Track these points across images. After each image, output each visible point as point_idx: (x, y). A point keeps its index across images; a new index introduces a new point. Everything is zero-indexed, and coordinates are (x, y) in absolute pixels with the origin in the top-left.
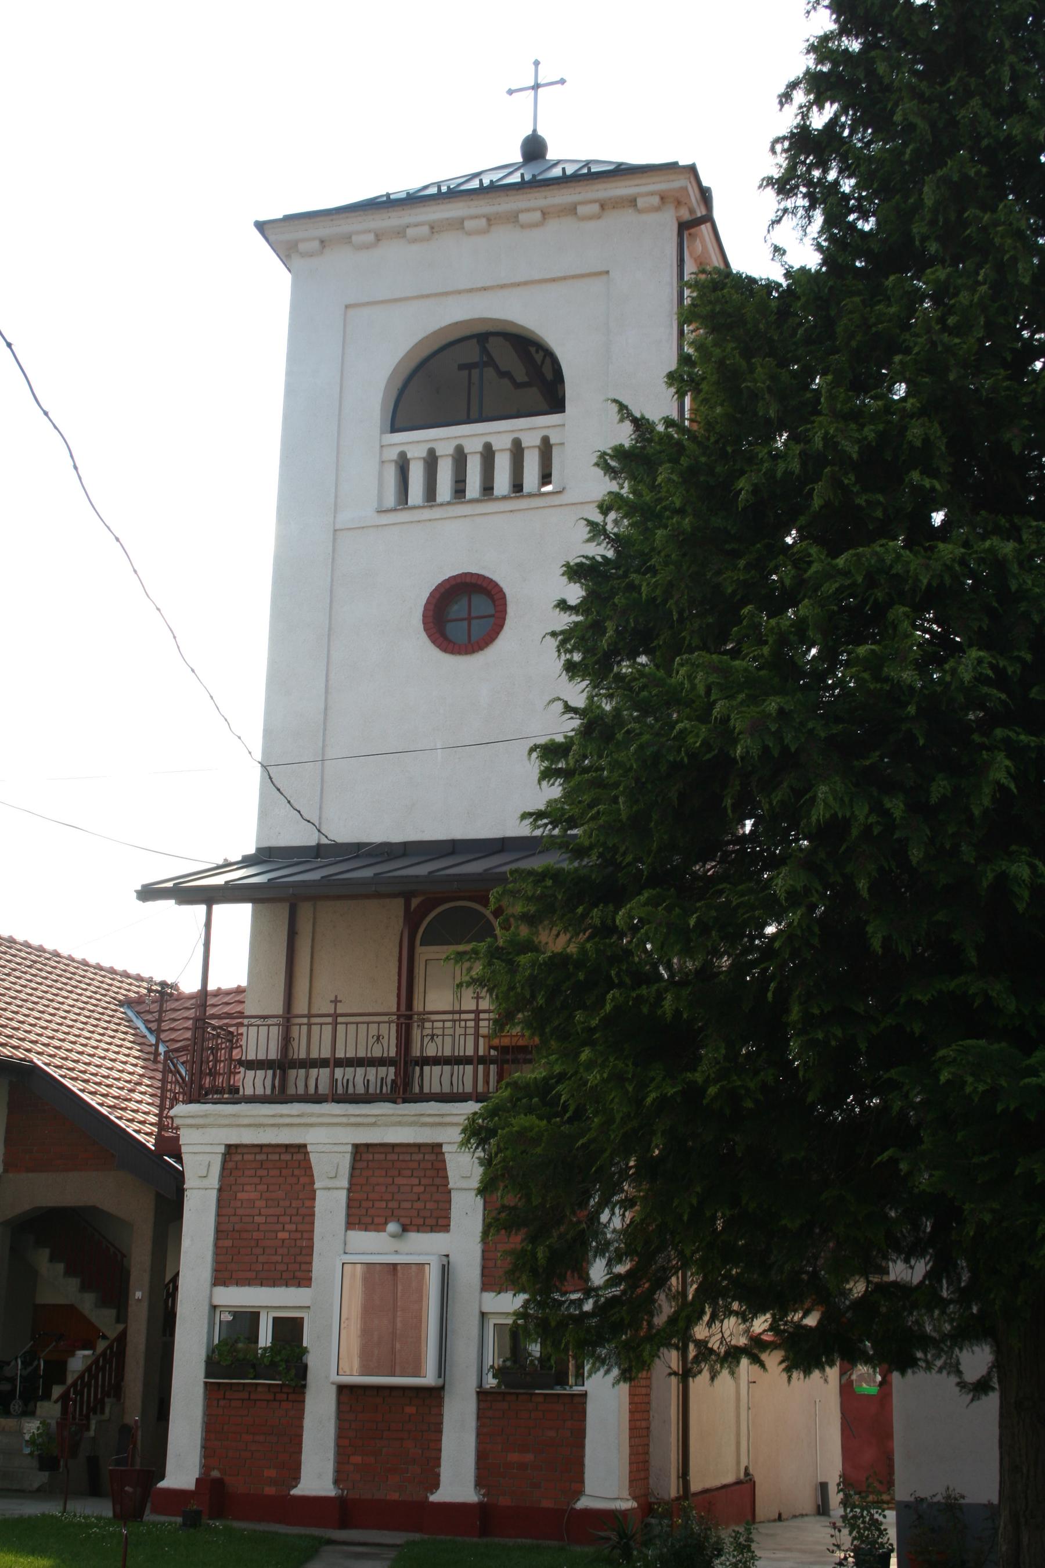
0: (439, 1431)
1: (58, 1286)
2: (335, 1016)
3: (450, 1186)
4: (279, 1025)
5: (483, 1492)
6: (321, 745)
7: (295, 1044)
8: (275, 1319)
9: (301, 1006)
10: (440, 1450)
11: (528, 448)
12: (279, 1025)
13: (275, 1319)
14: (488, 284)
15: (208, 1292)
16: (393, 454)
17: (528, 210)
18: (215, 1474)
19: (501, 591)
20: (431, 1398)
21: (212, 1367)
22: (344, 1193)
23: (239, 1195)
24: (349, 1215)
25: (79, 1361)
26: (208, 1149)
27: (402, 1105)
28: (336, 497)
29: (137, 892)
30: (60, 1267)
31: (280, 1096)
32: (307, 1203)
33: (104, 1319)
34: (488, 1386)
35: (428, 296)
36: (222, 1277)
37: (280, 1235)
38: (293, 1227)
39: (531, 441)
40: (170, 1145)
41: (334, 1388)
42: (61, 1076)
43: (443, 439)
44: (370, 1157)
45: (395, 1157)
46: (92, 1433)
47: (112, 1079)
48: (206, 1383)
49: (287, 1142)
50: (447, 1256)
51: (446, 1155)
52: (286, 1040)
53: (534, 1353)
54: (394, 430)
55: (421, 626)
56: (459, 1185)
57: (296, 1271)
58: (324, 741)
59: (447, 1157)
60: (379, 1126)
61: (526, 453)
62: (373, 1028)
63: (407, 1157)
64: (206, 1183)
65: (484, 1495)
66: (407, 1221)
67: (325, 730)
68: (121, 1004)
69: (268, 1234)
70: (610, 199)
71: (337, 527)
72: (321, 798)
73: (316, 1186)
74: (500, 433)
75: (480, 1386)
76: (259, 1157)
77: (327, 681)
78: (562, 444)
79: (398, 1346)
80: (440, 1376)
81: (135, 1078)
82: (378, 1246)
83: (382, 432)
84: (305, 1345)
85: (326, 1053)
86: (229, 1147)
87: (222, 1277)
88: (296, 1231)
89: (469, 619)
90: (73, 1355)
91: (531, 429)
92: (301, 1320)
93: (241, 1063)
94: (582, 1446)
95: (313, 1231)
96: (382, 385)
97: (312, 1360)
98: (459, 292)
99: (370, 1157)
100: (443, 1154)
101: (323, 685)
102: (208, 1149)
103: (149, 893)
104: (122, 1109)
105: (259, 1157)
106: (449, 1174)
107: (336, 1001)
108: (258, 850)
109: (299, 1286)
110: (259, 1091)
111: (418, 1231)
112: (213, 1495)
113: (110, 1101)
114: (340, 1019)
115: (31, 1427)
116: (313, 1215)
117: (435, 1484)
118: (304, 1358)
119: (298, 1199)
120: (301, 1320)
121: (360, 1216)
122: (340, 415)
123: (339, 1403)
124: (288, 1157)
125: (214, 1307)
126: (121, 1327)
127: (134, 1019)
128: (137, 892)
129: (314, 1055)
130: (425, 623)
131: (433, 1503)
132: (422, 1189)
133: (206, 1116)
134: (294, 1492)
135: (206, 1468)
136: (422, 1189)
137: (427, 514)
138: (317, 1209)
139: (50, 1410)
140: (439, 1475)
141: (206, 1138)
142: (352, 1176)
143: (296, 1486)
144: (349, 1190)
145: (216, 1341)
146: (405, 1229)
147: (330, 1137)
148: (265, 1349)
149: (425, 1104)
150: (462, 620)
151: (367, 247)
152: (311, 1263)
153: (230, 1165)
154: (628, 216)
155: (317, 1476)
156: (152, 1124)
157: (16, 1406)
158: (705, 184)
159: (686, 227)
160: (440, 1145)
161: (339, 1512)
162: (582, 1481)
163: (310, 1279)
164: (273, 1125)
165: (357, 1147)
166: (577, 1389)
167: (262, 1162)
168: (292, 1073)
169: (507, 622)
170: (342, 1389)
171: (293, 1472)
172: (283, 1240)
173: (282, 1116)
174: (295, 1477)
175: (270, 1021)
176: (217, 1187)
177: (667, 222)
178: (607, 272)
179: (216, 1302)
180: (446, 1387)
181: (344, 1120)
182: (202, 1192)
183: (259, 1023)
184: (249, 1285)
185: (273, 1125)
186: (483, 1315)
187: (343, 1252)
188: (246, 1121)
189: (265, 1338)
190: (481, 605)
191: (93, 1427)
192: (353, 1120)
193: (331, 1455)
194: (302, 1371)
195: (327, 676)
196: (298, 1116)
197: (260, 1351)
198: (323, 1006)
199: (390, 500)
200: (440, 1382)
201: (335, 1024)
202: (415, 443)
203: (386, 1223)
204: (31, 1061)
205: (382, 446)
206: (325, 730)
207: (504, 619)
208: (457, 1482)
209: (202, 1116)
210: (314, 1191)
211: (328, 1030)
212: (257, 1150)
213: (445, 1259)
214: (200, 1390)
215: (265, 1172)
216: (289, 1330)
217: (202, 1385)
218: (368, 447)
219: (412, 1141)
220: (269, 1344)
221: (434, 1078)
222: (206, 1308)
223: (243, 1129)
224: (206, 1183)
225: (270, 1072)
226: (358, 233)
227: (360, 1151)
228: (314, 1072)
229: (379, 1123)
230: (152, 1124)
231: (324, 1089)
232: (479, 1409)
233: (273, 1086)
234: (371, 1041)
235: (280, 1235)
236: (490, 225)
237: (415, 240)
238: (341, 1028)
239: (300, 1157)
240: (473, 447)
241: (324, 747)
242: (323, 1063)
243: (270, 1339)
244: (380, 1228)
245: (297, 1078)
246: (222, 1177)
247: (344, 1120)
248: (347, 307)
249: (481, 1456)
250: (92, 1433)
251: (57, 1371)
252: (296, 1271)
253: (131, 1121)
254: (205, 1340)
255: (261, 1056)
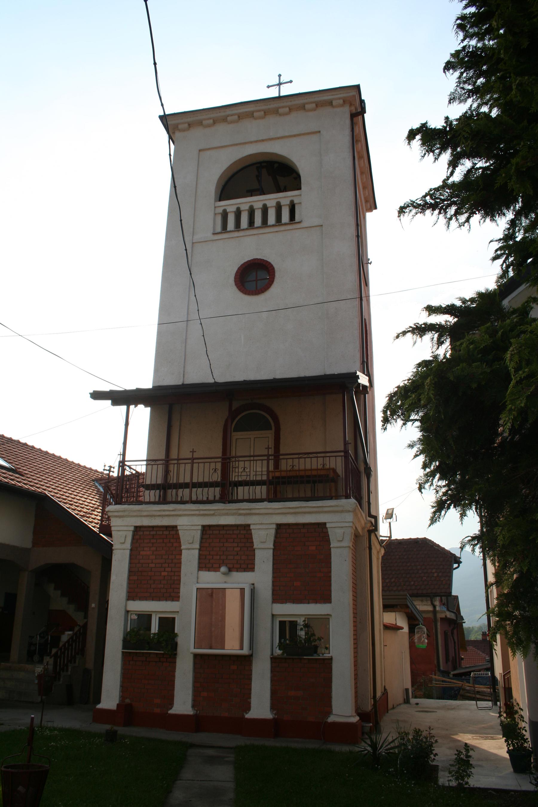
0: (250, 679)
1: (59, 602)
2: (193, 459)
3: (255, 547)
4: (163, 464)
5: (275, 712)
6: (184, 337)
7: (171, 474)
8: (160, 618)
9: (174, 454)
10: (251, 689)
11: (284, 205)
12: (163, 464)
13: (160, 618)
14: (264, 138)
15: (124, 604)
16: (220, 210)
17: (283, 107)
18: (128, 701)
19: (272, 266)
20: (245, 661)
21: (127, 643)
22: (197, 552)
23: (141, 553)
24: (199, 563)
25: (66, 636)
26: (125, 528)
27: (228, 505)
28: (193, 229)
29: (90, 394)
30: (59, 592)
31: (163, 501)
32: (177, 557)
33: (78, 617)
34: (276, 654)
35: (237, 145)
36: (132, 595)
37: (163, 574)
38: (170, 569)
39: (285, 202)
40: (106, 529)
41: (192, 656)
42: (52, 496)
43: (244, 203)
44: (211, 532)
45: (224, 532)
46: (69, 673)
47: (86, 508)
48: (123, 652)
49: (167, 524)
50: (253, 584)
51: (252, 531)
52: (167, 472)
53: (302, 636)
54: (220, 200)
55: (233, 283)
56: (260, 546)
57: (172, 593)
58: (186, 336)
59: (253, 532)
60: (216, 516)
61: (283, 208)
62: (213, 465)
63: (231, 532)
64: (124, 546)
65: (275, 714)
66: (231, 566)
67: (187, 331)
68: (93, 480)
69: (156, 570)
70: (320, 101)
71: (194, 241)
72: (185, 363)
73: (182, 548)
74: (271, 199)
75: (272, 654)
76: (152, 533)
77: (188, 309)
78: (300, 203)
79: (213, 629)
80: (250, 649)
81: (96, 506)
82: (211, 579)
83: (215, 201)
84: (176, 632)
85: (188, 480)
86: (136, 527)
87: (132, 595)
88: (171, 571)
89: (256, 280)
90: (64, 634)
91: (285, 198)
92: (174, 619)
93: (143, 486)
94: (330, 687)
95: (180, 571)
96: (216, 182)
97: (180, 640)
98: (251, 142)
99: (211, 532)
100: (251, 530)
101: (186, 311)
102: (125, 528)
103: (97, 395)
104: (87, 517)
105: (152, 533)
106: (254, 541)
107: (193, 452)
108: (153, 387)
109: (173, 600)
110: (152, 500)
111: (237, 571)
112: (126, 712)
113: (82, 514)
114: (195, 461)
115: (39, 669)
116: (180, 563)
117: (248, 708)
118: (176, 639)
119: (172, 554)
120: (174, 619)
121: (206, 563)
122: (196, 194)
123: (195, 663)
124: (167, 533)
125: (127, 612)
126: (85, 620)
127: (98, 486)
128: (90, 394)
129: (181, 481)
130: (235, 281)
131: (247, 719)
132: (239, 549)
133: (124, 511)
134: (170, 712)
135: (123, 697)
136: (239, 549)
137: (236, 234)
138: (182, 560)
139: (49, 660)
140: (250, 703)
141: (125, 523)
142: (201, 542)
143: (171, 708)
144: (200, 550)
145: (129, 630)
146: (230, 570)
147: (189, 522)
148: (154, 634)
149: (241, 503)
150: (254, 281)
151: (209, 126)
152: (179, 588)
153: (137, 537)
154: (328, 110)
155: (183, 703)
156: (98, 520)
157: (36, 658)
158: (363, 98)
159: (353, 116)
160: (249, 526)
161: (194, 723)
162: (331, 706)
163: (179, 597)
164: (159, 516)
165: (204, 527)
166: (327, 656)
167: (153, 535)
168: (169, 491)
169: (276, 280)
170: (196, 656)
171: (170, 701)
172: (165, 576)
173: (164, 511)
174: (171, 704)
175: (158, 463)
176: (130, 548)
177: (345, 112)
178: (320, 132)
179: (129, 609)
180: (254, 655)
181: (197, 512)
182: (122, 551)
183: (153, 463)
184: (146, 600)
185: (159, 516)
186: (273, 615)
187: (193, 579)
188: (145, 514)
189: (155, 628)
190: (262, 274)
191: (70, 670)
192: (202, 512)
193: (190, 692)
194: (175, 646)
195: (188, 307)
196: (173, 510)
197: (152, 635)
198: (186, 453)
199: (219, 229)
200: (251, 652)
201: (193, 463)
202: (230, 205)
203: (220, 567)
204: (45, 494)
205: (215, 207)
206: (187, 331)
207: (274, 278)
208: (260, 707)
209: (122, 511)
210: (181, 551)
211: (188, 467)
212: (151, 529)
213: (252, 586)
214: (119, 655)
215: (155, 541)
216: (167, 624)
217: (121, 653)
218: (207, 211)
219: (234, 523)
220: (157, 632)
221: (242, 492)
222: (123, 613)
223: (143, 518)
224: (124, 546)
225: (158, 491)
226: (205, 119)
227: (205, 529)
228: (180, 491)
229: (216, 514)
230: (98, 520)
231: (186, 498)
232: (272, 667)
233: (160, 496)
234: (211, 472)
235: (163, 574)
236: (265, 115)
237: (232, 122)
238: (195, 465)
239: (174, 532)
240: (258, 206)
241: (186, 339)
242: (185, 486)
243: (157, 629)
244: (217, 569)
245: (171, 493)
246: (132, 543)
247: (197, 512)
248: (200, 151)
249: (274, 693)
250: (69, 673)
251: (56, 640)
252: (172, 593)
253: (91, 522)
254: (122, 629)
255: (154, 482)
